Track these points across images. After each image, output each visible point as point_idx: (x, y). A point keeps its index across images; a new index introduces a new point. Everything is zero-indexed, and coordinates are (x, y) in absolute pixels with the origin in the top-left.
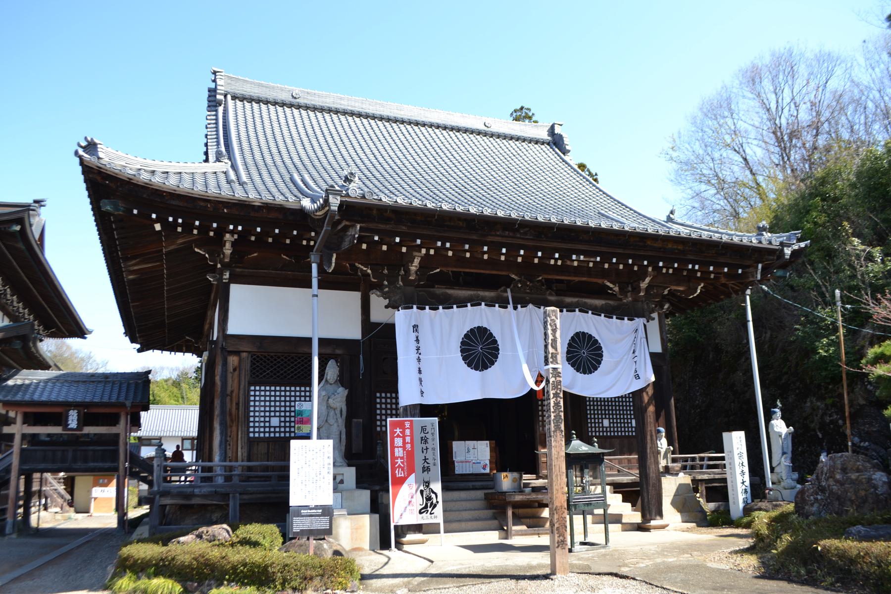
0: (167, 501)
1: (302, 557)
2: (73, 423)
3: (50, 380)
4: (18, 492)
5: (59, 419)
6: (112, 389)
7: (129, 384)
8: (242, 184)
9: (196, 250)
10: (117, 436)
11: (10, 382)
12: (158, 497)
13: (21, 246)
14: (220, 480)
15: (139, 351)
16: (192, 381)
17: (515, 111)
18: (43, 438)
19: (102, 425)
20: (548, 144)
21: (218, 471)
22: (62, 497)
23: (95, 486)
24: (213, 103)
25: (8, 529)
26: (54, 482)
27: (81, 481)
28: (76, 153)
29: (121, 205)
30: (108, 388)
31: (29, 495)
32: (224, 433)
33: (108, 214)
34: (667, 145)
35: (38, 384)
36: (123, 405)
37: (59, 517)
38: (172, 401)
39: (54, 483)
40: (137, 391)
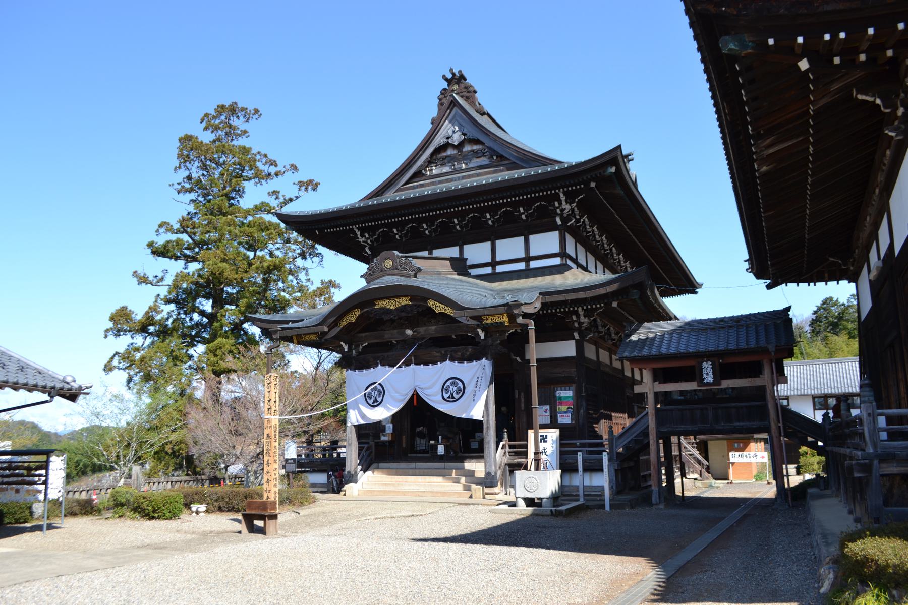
2: (709, 378)
3: (674, 330)
4: (659, 457)
5: (693, 374)
6: (747, 333)
7: (766, 326)
9: (860, 97)
10: (762, 389)
11: (634, 338)
12: (876, 462)
13: (620, 191)
15: (769, 287)
16: (809, 335)
18: (676, 397)
19: (740, 377)
22: (699, 462)
23: (730, 451)
25: (655, 498)
26: (689, 447)
27: (716, 446)
29: (747, 38)
30: (743, 332)
31: (669, 461)
33: (733, 58)
35: (663, 336)
36: (765, 351)
37: (699, 484)
39: (688, 448)
40: (772, 338)
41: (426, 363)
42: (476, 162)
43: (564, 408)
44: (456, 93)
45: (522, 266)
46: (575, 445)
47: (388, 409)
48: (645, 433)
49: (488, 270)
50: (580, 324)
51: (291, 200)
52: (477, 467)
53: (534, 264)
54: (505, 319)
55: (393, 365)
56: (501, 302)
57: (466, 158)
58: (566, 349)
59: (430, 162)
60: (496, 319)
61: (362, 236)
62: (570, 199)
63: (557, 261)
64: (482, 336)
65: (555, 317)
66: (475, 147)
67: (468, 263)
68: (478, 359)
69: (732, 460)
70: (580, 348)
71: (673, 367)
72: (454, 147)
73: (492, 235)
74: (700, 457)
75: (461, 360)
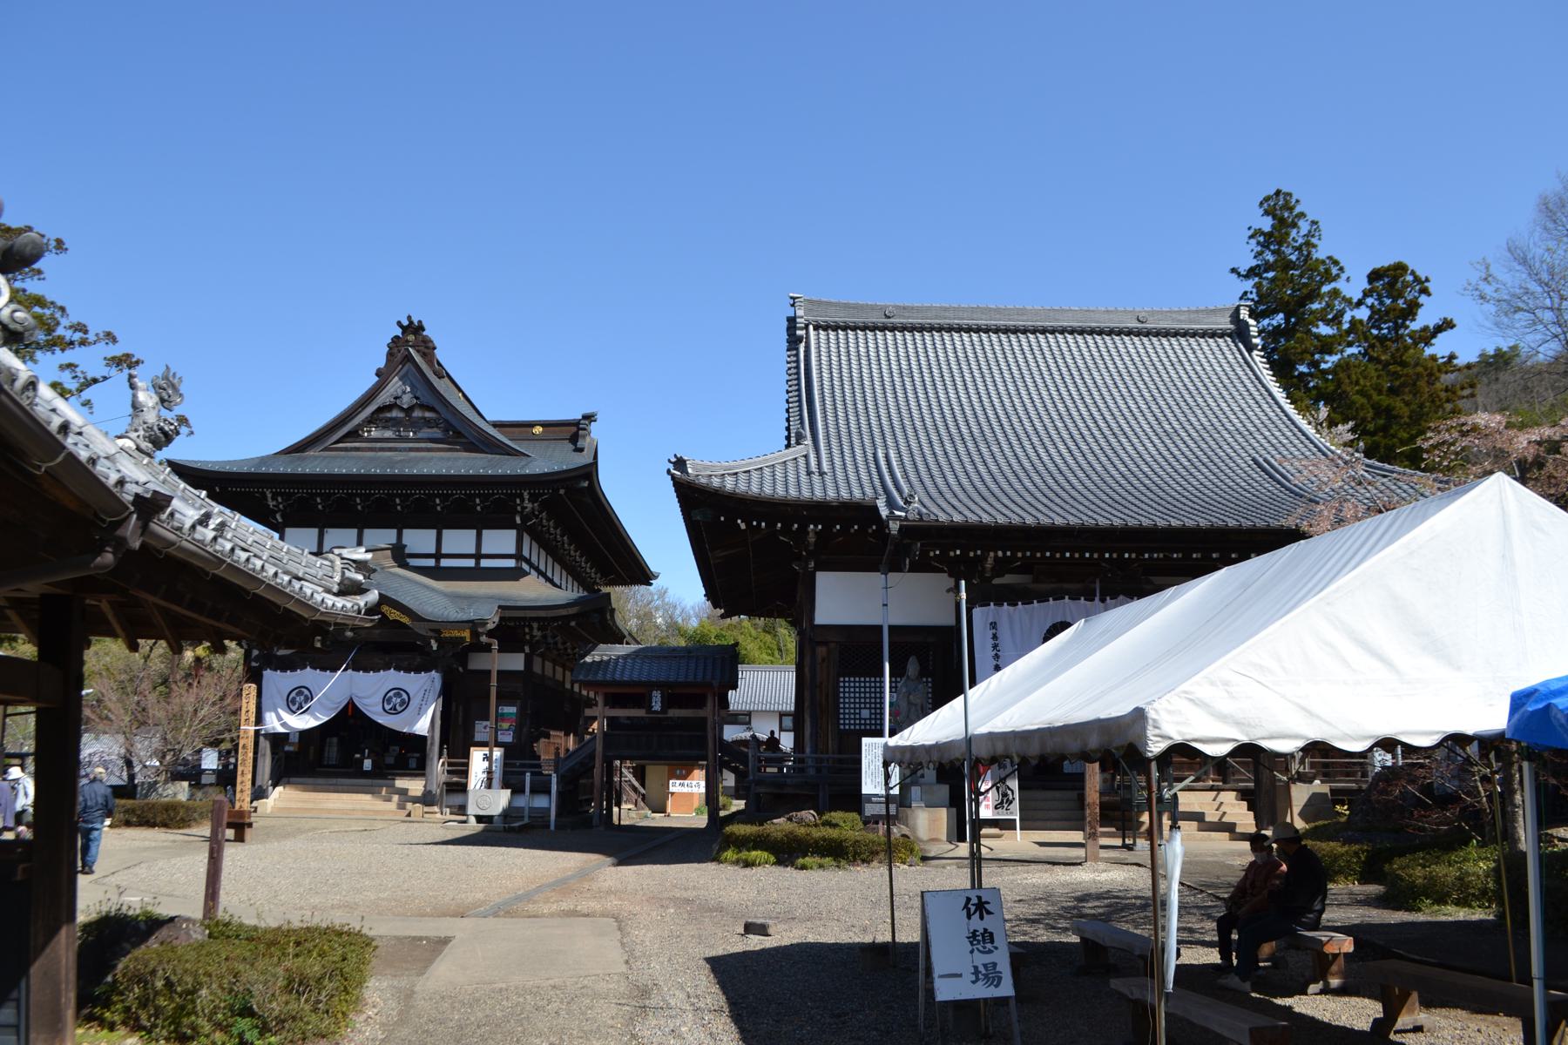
0: (762, 790)
1: (871, 836)
2: (657, 707)
5: (642, 701)
8: (822, 474)
10: (704, 720)
11: (588, 659)
14: (812, 772)
15: (723, 617)
17: (1267, 199)
20: (1230, 335)
21: (810, 762)
22: (635, 789)
24: (793, 341)
27: (654, 772)
28: (669, 472)
32: (814, 725)
34: (1475, 276)
38: (765, 656)
41: (366, 670)
42: (426, 432)
43: (505, 725)
44: (410, 348)
45: (471, 563)
46: (523, 766)
47: (317, 718)
48: (592, 756)
49: (431, 562)
50: (532, 637)
51: (95, 381)
52: (415, 786)
53: (485, 563)
54: (467, 634)
55: (334, 669)
56: (465, 618)
57: (415, 425)
58: (516, 662)
59: (371, 421)
60: (456, 634)
61: (273, 499)
62: (533, 499)
63: (511, 563)
64: (435, 646)
65: (514, 627)
66: (428, 414)
67: (407, 551)
68: (428, 670)
69: (672, 789)
70: (528, 662)
71: (623, 693)
72: (402, 409)
73: (440, 523)
74: (636, 784)
75: (408, 671)
